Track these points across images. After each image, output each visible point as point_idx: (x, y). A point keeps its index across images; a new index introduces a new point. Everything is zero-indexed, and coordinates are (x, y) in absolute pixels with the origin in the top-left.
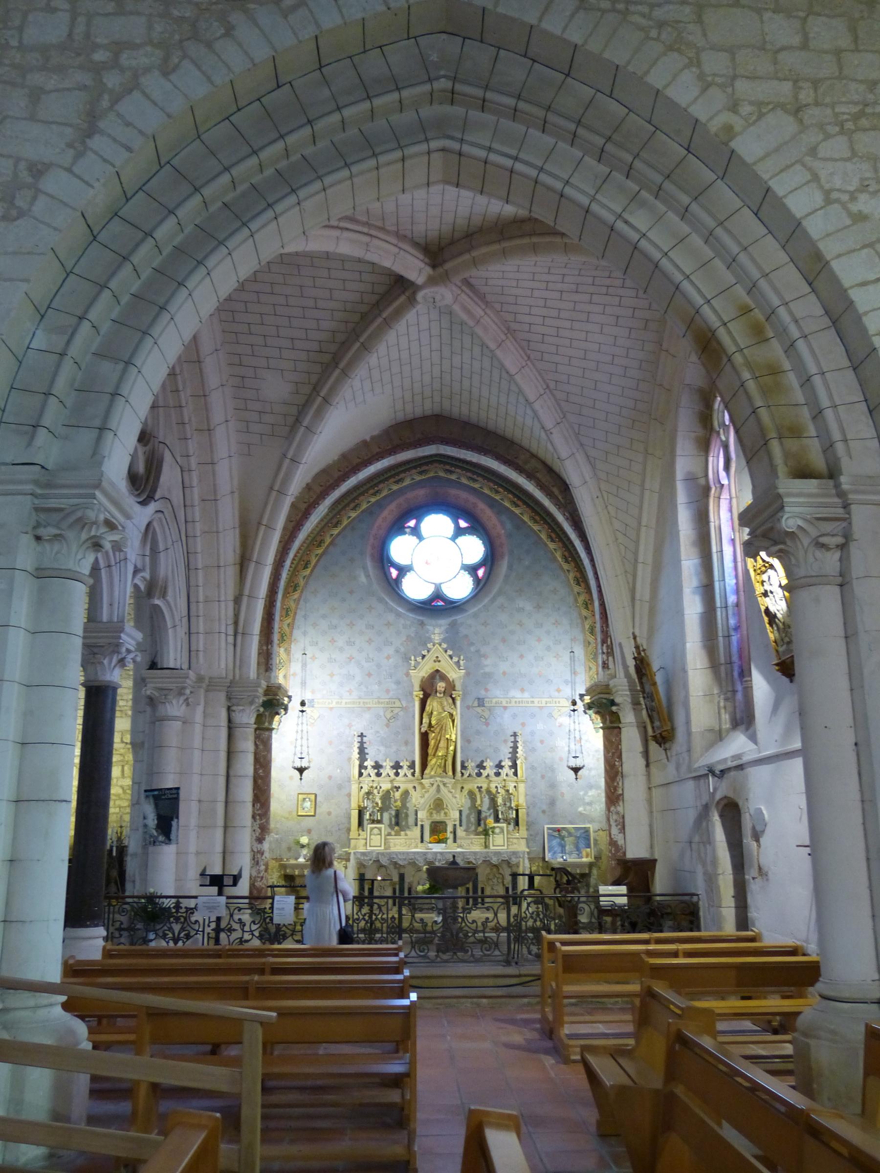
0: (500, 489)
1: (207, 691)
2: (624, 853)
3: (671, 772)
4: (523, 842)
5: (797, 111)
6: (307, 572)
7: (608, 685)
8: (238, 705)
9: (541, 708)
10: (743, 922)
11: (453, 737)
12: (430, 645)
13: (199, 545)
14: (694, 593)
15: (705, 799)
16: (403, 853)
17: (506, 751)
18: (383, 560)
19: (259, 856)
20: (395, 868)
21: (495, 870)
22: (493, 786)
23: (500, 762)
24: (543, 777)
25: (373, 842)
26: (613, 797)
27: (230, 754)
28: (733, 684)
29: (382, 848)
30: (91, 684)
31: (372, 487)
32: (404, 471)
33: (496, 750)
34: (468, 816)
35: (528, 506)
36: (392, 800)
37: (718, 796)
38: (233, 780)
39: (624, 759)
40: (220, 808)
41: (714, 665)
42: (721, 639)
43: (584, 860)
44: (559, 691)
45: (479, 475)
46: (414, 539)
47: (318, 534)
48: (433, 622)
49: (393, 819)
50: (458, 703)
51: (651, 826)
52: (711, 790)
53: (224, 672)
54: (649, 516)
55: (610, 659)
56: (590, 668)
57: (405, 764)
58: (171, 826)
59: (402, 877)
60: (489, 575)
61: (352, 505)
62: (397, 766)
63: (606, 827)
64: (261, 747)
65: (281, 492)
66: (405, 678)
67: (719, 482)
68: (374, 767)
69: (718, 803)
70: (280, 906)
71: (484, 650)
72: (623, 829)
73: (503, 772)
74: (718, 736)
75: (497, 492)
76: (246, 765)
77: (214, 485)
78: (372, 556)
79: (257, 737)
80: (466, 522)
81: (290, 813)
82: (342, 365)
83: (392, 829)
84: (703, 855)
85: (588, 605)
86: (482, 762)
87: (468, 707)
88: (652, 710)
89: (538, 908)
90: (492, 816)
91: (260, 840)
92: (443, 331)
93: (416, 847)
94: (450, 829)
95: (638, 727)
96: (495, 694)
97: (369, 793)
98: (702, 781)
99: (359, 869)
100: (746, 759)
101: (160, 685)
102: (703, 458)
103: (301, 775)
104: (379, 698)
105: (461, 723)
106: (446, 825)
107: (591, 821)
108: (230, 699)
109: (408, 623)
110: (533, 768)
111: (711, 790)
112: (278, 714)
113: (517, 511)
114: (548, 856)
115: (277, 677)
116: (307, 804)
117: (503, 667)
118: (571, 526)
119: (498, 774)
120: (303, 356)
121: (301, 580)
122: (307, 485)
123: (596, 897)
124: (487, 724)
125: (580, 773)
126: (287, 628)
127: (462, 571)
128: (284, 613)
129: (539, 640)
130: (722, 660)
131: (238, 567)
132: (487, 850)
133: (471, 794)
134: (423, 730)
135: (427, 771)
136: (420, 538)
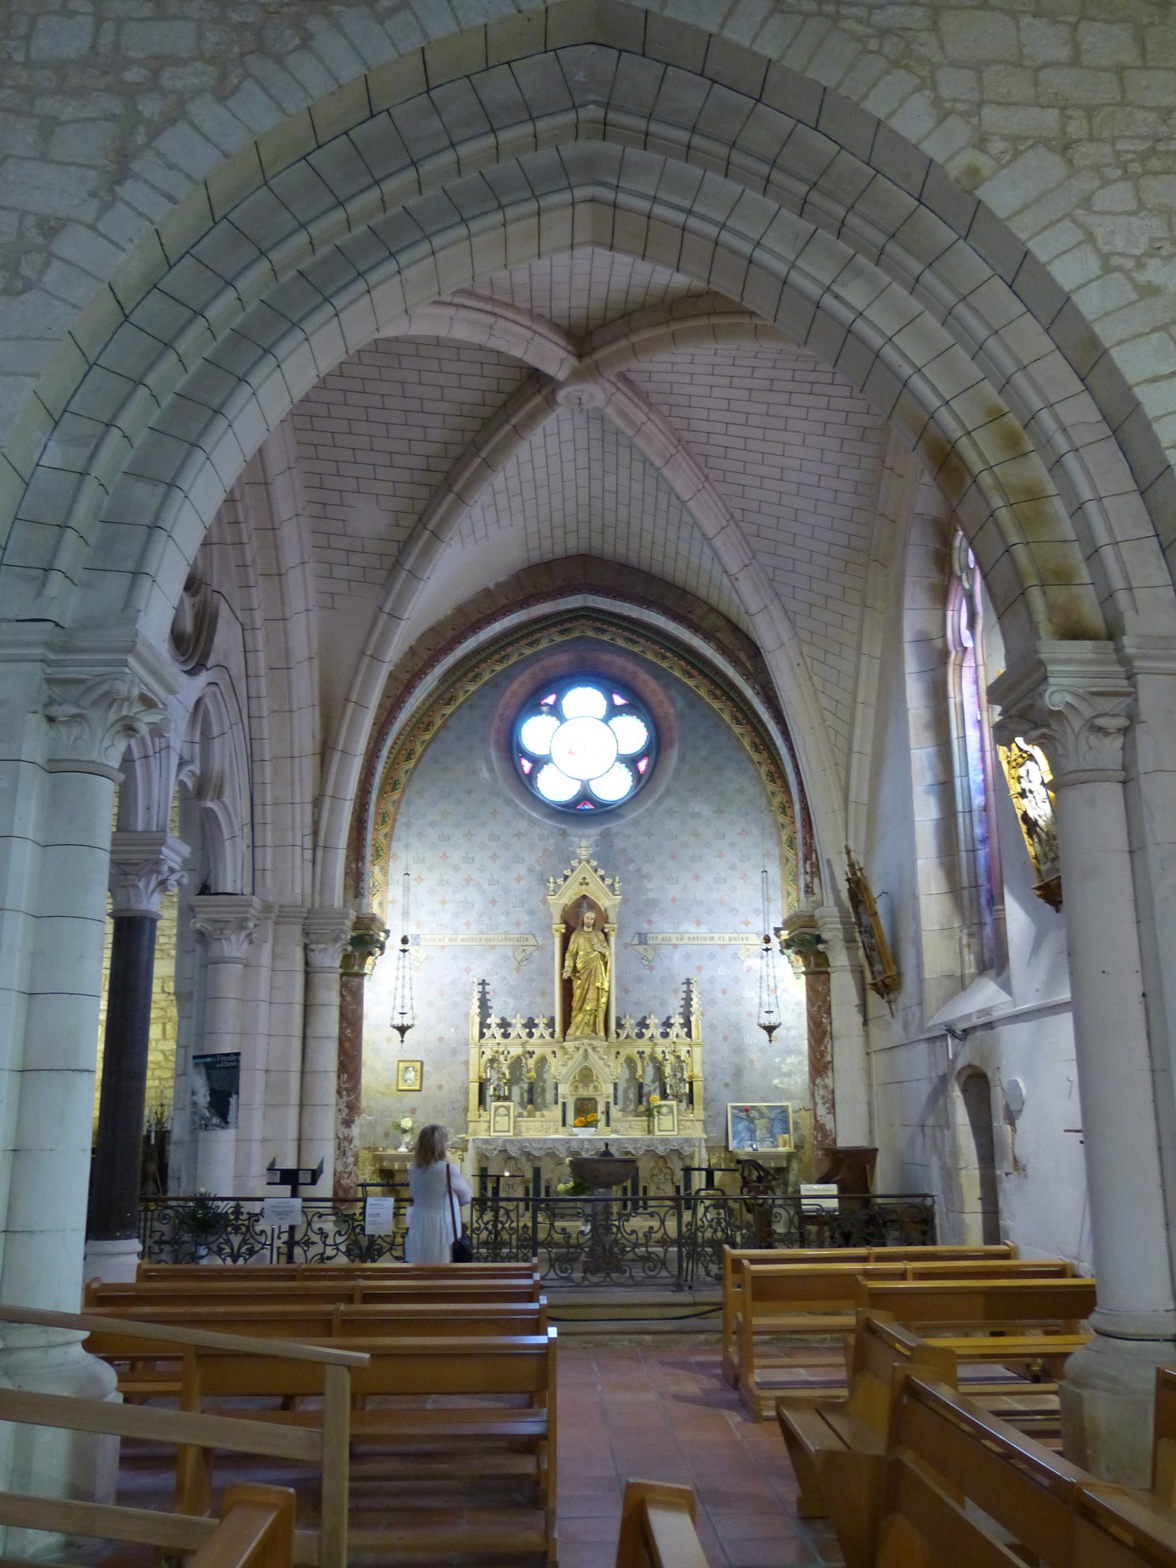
0: (668, 654)
1: (276, 924)
2: (835, 1141)
3: (896, 1032)
4: (699, 1126)
5: (1065, 148)
6: (411, 764)
7: (812, 916)
8: (318, 943)
9: (723, 946)
10: (993, 1232)
11: (606, 986)
12: (574, 863)
13: (266, 728)
14: (927, 793)
15: (943, 1068)
16: (539, 1140)
17: (676, 1003)
18: (512, 749)
19: (346, 1144)
20: (528, 1160)
21: (661, 1163)
22: (659, 1050)
23: (669, 1018)
24: (725, 1038)
25: (499, 1125)
26: (820, 1065)
27: (308, 1007)
28: (980, 914)
29: (511, 1133)
30: (122, 914)
31: (497, 651)
32: (540, 630)
33: (663, 1003)
34: (626, 1091)
35: (706, 676)
36: (524, 1069)
37: (960, 1065)
38: (311, 1043)
39: (834, 1015)
40: (294, 1080)
41: (954, 889)
42: (963, 854)
43: (781, 1149)
44: (746, 923)
45: (640, 635)
46: (553, 721)
47: (426, 714)
48: (579, 831)
49: (525, 1095)
50: (612, 939)
51: (870, 1104)
52: (951, 1057)
53: (299, 899)
54: (867, 690)
55: (816, 880)
56: (789, 893)
57: (541, 1021)
58: (228, 1104)
59: (537, 1172)
60: (653, 769)
61: (471, 675)
62: (530, 1024)
63: (809, 1105)
64: (349, 999)
65: (376, 658)
66: (542, 907)
67: (961, 644)
68: (500, 1026)
69: (959, 1073)
70: (375, 1212)
71: (646, 869)
72: (832, 1109)
73: (672, 1032)
74: (960, 984)
75: (664, 658)
76: (329, 1023)
77: (287, 648)
78: (498, 743)
79: (344, 986)
80: (623, 697)
81: (388, 1086)
82: (457, 488)
83: (524, 1108)
84: (939, 1143)
85: (785, 808)
86: (645, 1018)
87: (626, 946)
88: (872, 949)
89: (719, 1214)
90: (658, 1091)
91: (348, 1123)
92: (593, 443)
93: (556, 1132)
94: (601, 1107)
95: (852, 971)
96: (662, 928)
97: (493, 1061)
98: (938, 1044)
99: (479, 1161)
100: (997, 1014)
101: (214, 916)
102: (940, 613)
103: (402, 1035)
104: (506, 933)
105: (617, 966)
106: (596, 1103)
107: (790, 1098)
108: (307, 934)
109: (546, 832)
110: (712, 1027)
111: (951, 1057)
112: (371, 954)
113: (691, 683)
114: (732, 1145)
115: (370, 905)
116: (411, 1075)
117: (673, 891)
118: (763, 703)
119: (665, 1035)
120: (405, 476)
121: (403, 775)
122: (411, 648)
123: (797, 1198)
124: (651, 968)
125: (775, 1033)
126: (383, 840)
127: (618, 764)
128: (379, 820)
129: (720, 856)
130: (965, 883)
131: (318, 758)
132: (651, 1136)
133: (630, 1061)
134: (566, 976)
135: (570, 1031)
136: (562, 719)
